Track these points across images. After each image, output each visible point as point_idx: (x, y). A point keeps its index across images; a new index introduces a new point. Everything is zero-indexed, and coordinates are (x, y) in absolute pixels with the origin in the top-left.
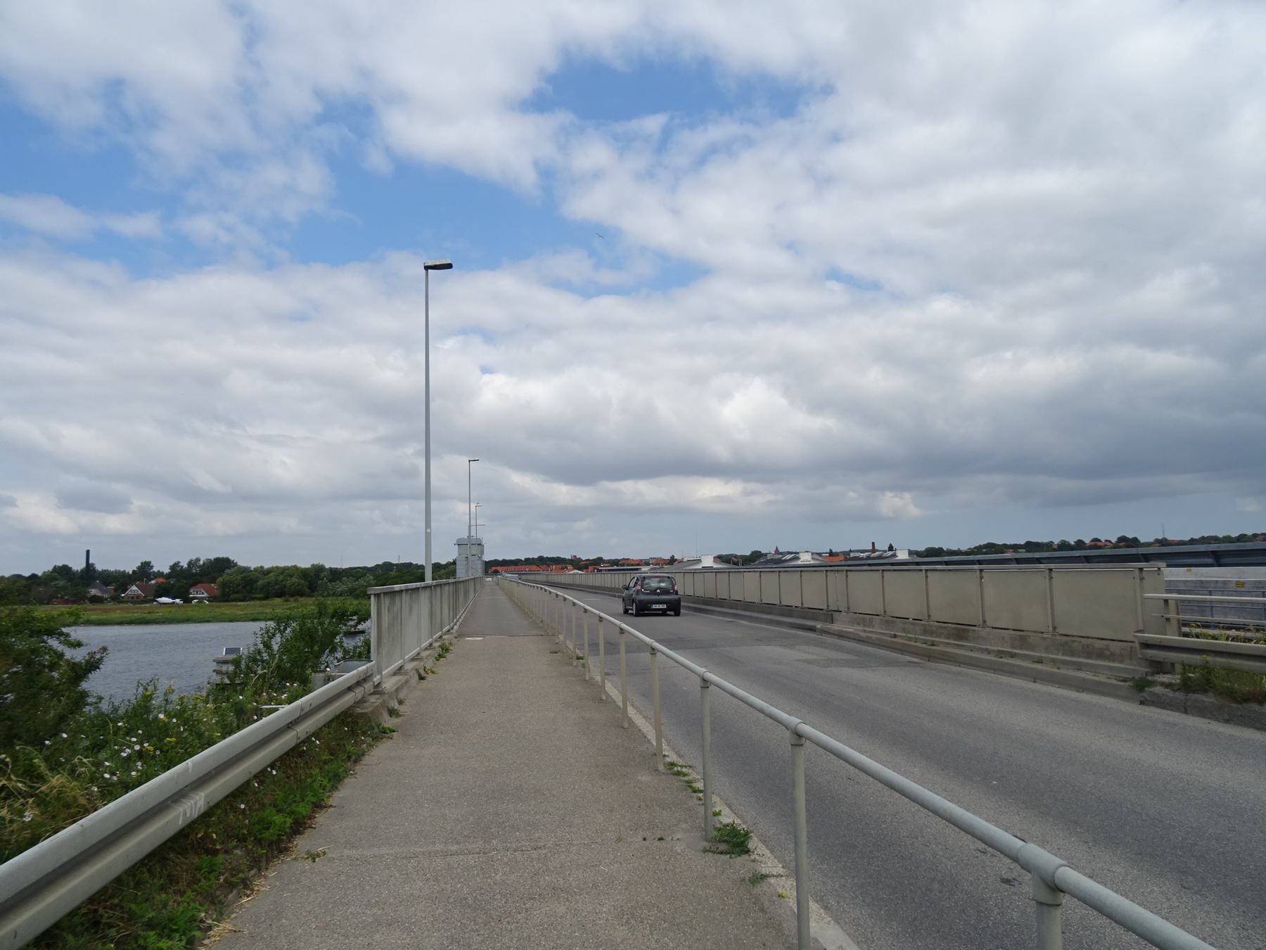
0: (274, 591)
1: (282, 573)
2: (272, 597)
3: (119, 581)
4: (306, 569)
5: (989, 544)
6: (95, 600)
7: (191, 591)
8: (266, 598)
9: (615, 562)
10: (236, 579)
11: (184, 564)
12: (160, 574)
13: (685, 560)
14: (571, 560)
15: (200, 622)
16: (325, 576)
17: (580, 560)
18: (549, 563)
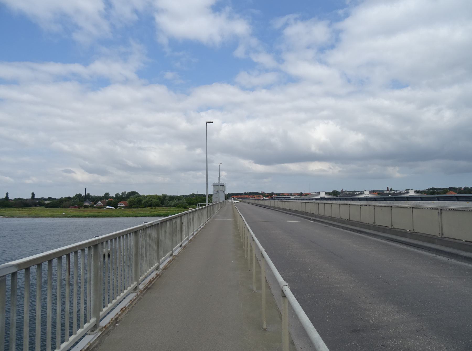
0: (148, 204)
1: (151, 197)
2: (148, 207)
3: (95, 199)
4: (160, 196)
5: (432, 188)
6: (86, 207)
7: (118, 204)
8: (145, 207)
9: (279, 195)
10: (135, 200)
11: (120, 194)
12: (112, 197)
13: (312, 194)
14: (262, 193)
15: (115, 217)
16: (167, 199)
17: (265, 193)
18: (253, 194)
